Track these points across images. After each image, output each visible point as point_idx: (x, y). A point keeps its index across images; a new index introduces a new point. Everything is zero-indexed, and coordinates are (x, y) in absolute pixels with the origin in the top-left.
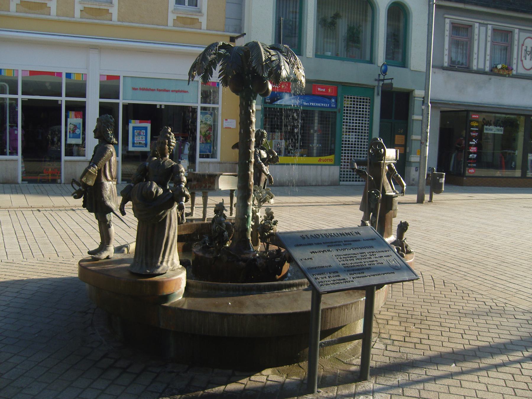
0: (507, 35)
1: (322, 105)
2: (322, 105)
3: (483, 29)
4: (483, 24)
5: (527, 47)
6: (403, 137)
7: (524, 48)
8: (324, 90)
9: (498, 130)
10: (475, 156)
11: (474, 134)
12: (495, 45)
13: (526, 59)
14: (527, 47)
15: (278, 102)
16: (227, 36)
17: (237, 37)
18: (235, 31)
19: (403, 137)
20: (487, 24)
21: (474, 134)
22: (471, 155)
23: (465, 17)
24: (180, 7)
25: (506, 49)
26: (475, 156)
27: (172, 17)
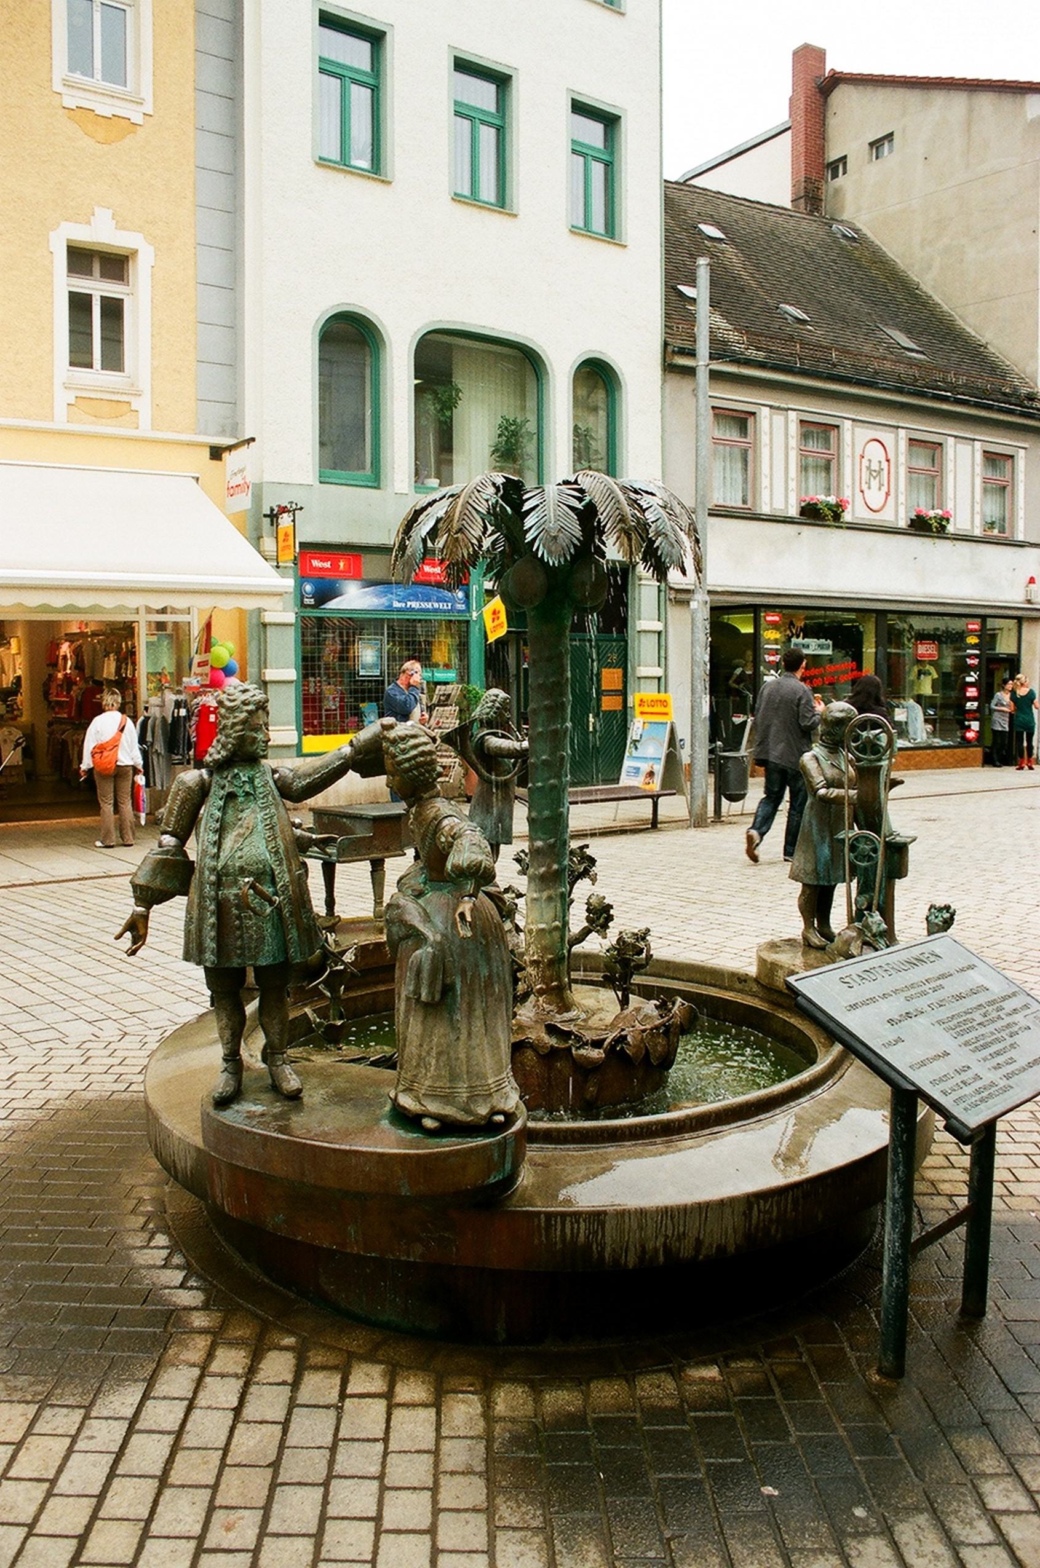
0: (935, 448)
1: (436, 605)
2: (436, 605)
3: (779, 419)
4: (779, 408)
5: (870, 461)
6: (619, 672)
7: (865, 462)
8: (328, 565)
9: (821, 646)
10: (976, 704)
11: (972, 662)
12: (806, 457)
13: (869, 488)
14: (870, 461)
15: (332, 604)
16: (201, 445)
17: (230, 448)
18: (223, 433)
19: (619, 672)
20: (974, 440)
21: (972, 662)
22: (969, 704)
23: (914, 422)
24: (82, 374)
25: (827, 468)
26: (976, 704)
27: (62, 398)
